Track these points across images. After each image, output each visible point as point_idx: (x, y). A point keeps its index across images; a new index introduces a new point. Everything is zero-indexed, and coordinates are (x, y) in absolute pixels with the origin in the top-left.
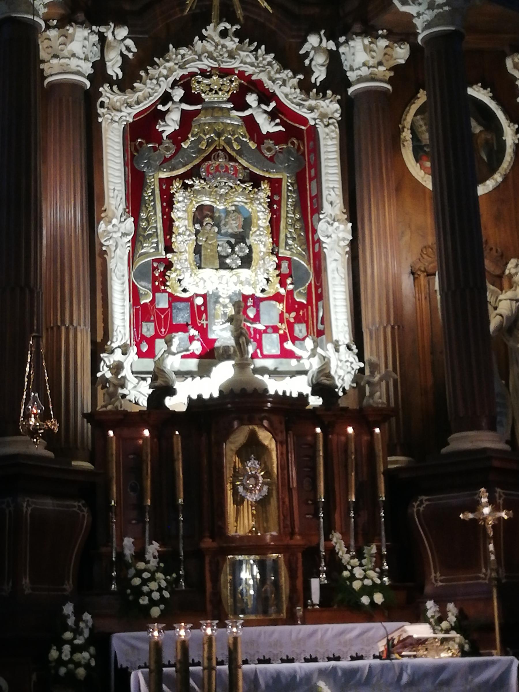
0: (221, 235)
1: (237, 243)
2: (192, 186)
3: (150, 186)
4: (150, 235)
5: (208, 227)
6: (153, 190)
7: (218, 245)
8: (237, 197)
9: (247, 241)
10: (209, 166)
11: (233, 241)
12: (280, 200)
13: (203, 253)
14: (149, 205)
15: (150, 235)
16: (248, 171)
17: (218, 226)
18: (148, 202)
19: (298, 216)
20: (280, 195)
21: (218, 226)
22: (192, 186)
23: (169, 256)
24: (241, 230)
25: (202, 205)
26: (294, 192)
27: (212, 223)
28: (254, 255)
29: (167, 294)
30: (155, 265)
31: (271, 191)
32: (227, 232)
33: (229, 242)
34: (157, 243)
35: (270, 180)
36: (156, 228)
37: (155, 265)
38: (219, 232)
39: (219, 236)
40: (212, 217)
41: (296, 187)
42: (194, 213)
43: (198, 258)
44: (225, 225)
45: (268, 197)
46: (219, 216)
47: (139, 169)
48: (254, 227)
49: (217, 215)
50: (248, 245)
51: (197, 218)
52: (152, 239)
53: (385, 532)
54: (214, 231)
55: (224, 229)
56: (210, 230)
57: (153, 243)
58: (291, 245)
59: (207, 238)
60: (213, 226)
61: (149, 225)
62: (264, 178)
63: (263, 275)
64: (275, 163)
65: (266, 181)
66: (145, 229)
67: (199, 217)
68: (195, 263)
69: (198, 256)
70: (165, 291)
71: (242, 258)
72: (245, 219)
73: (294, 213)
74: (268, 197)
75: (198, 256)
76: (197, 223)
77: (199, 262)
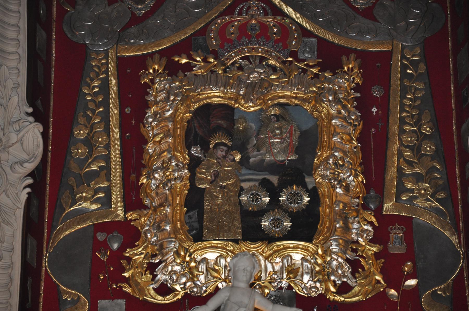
0: (249, 167)
1: (284, 185)
2: (188, 67)
3: (98, 74)
4: (95, 175)
5: (220, 153)
6: (105, 83)
7: (242, 189)
8: (283, 88)
9: (308, 180)
10: (225, 26)
11: (274, 179)
12: (386, 98)
13: (207, 207)
14: (93, 112)
15: (95, 175)
16: (313, 40)
17: (242, 148)
18: (91, 106)
19: (427, 130)
20: (387, 87)
21: (242, 148)
22: (188, 67)
23: (132, 216)
24: (292, 157)
25: (209, 105)
26: (419, 78)
27: (230, 144)
28: (324, 211)
29: (123, 302)
30: (101, 237)
31: (364, 76)
32: (263, 161)
33: (265, 184)
34: (108, 191)
35: (360, 55)
36: (107, 159)
37: (101, 237)
38: (244, 162)
39: (244, 171)
40: (229, 133)
41: (422, 69)
42: (188, 122)
43: (195, 218)
44: (258, 148)
45: (357, 88)
46: (244, 127)
47: (74, 40)
48: (322, 150)
49: (240, 126)
50: (310, 187)
51: (196, 134)
52: (96, 183)
53: (83, 228)
54: (234, 160)
55: (255, 156)
56: (224, 157)
57: (97, 191)
58: (412, 191)
59: (216, 175)
60: (230, 149)
61: (91, 153)
62: (347, 51)
63: (345, 253)
64: (376, 20)
65: (352, 56)
66: (83, 163)
67: (199, 132)
68: (187, 228)
69: (194, 213)
70: (120, 294)
71: (293, 216)
72: (304, 135)
73: (418, 124)
74: (357, 88)
75: (194, 213)
76: (195, 145)
77: (196, 225)
